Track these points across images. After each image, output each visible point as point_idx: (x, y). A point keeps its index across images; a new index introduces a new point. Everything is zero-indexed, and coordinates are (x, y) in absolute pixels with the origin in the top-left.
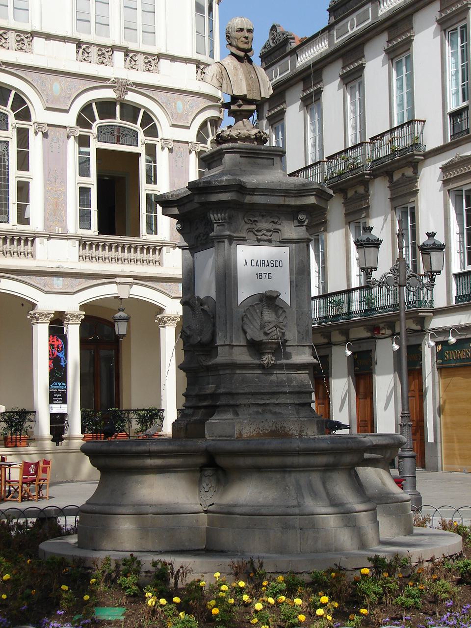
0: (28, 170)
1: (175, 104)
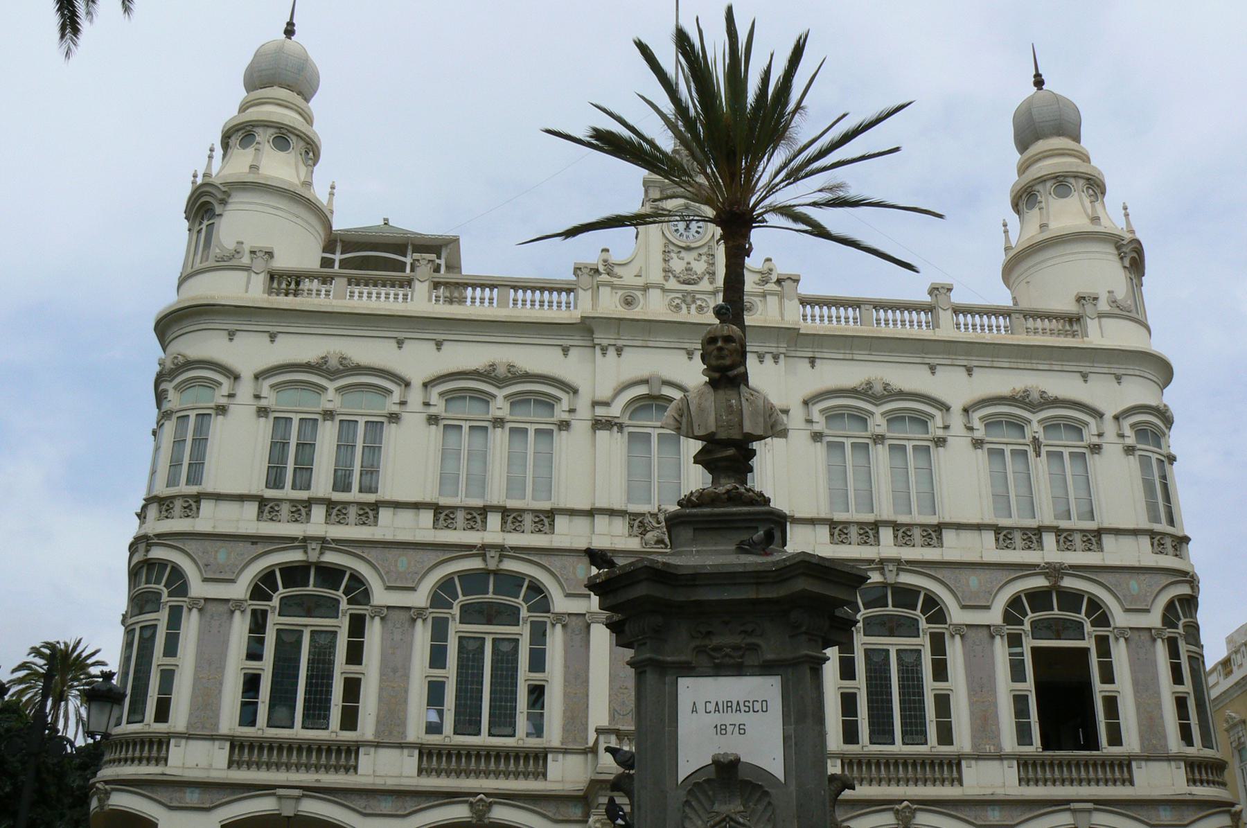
0: (947, 680)
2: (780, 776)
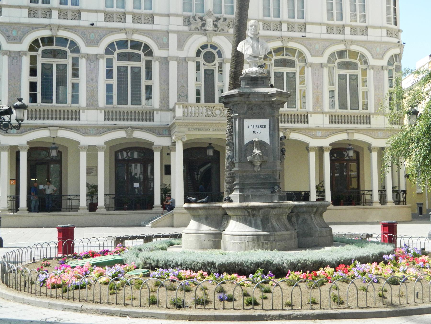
2: (269, 143)
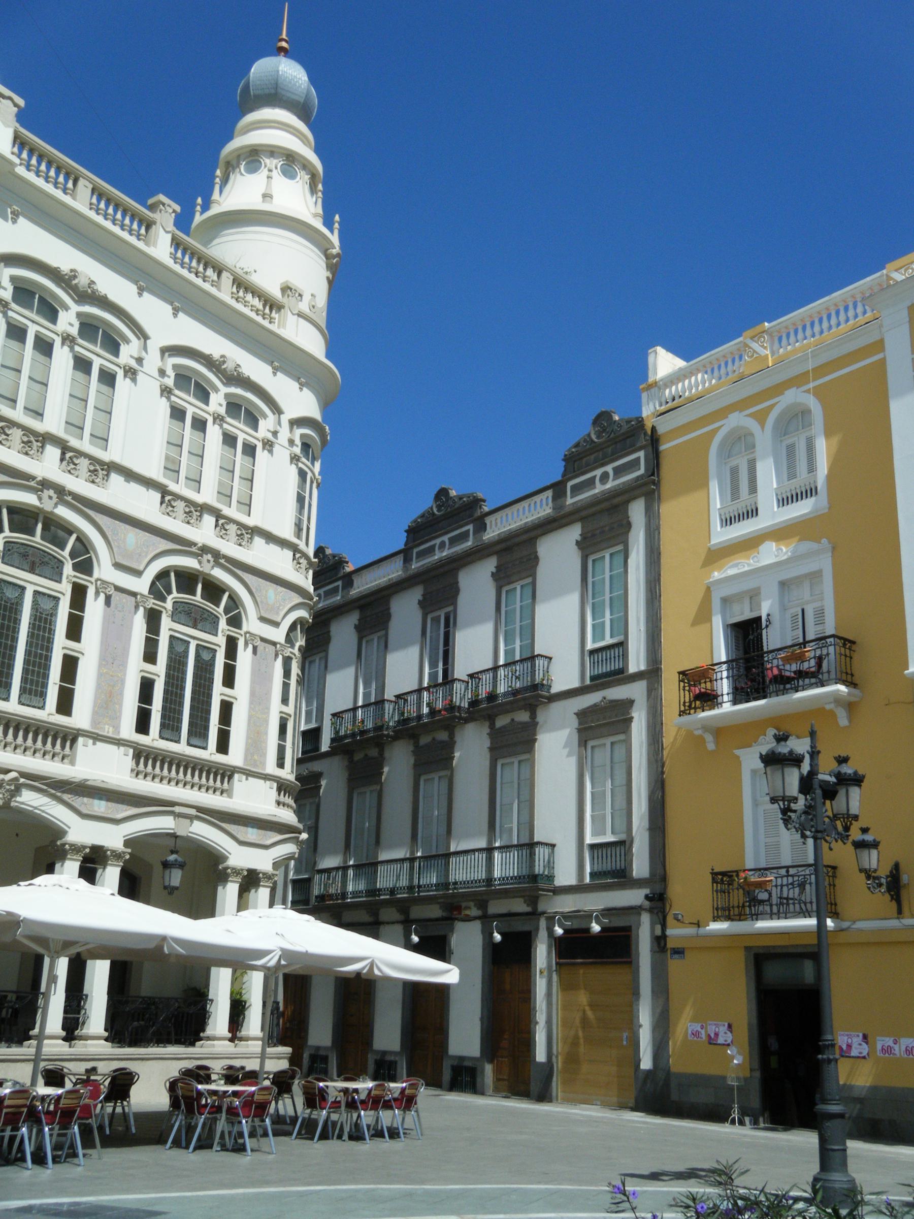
1: (266, 591)
